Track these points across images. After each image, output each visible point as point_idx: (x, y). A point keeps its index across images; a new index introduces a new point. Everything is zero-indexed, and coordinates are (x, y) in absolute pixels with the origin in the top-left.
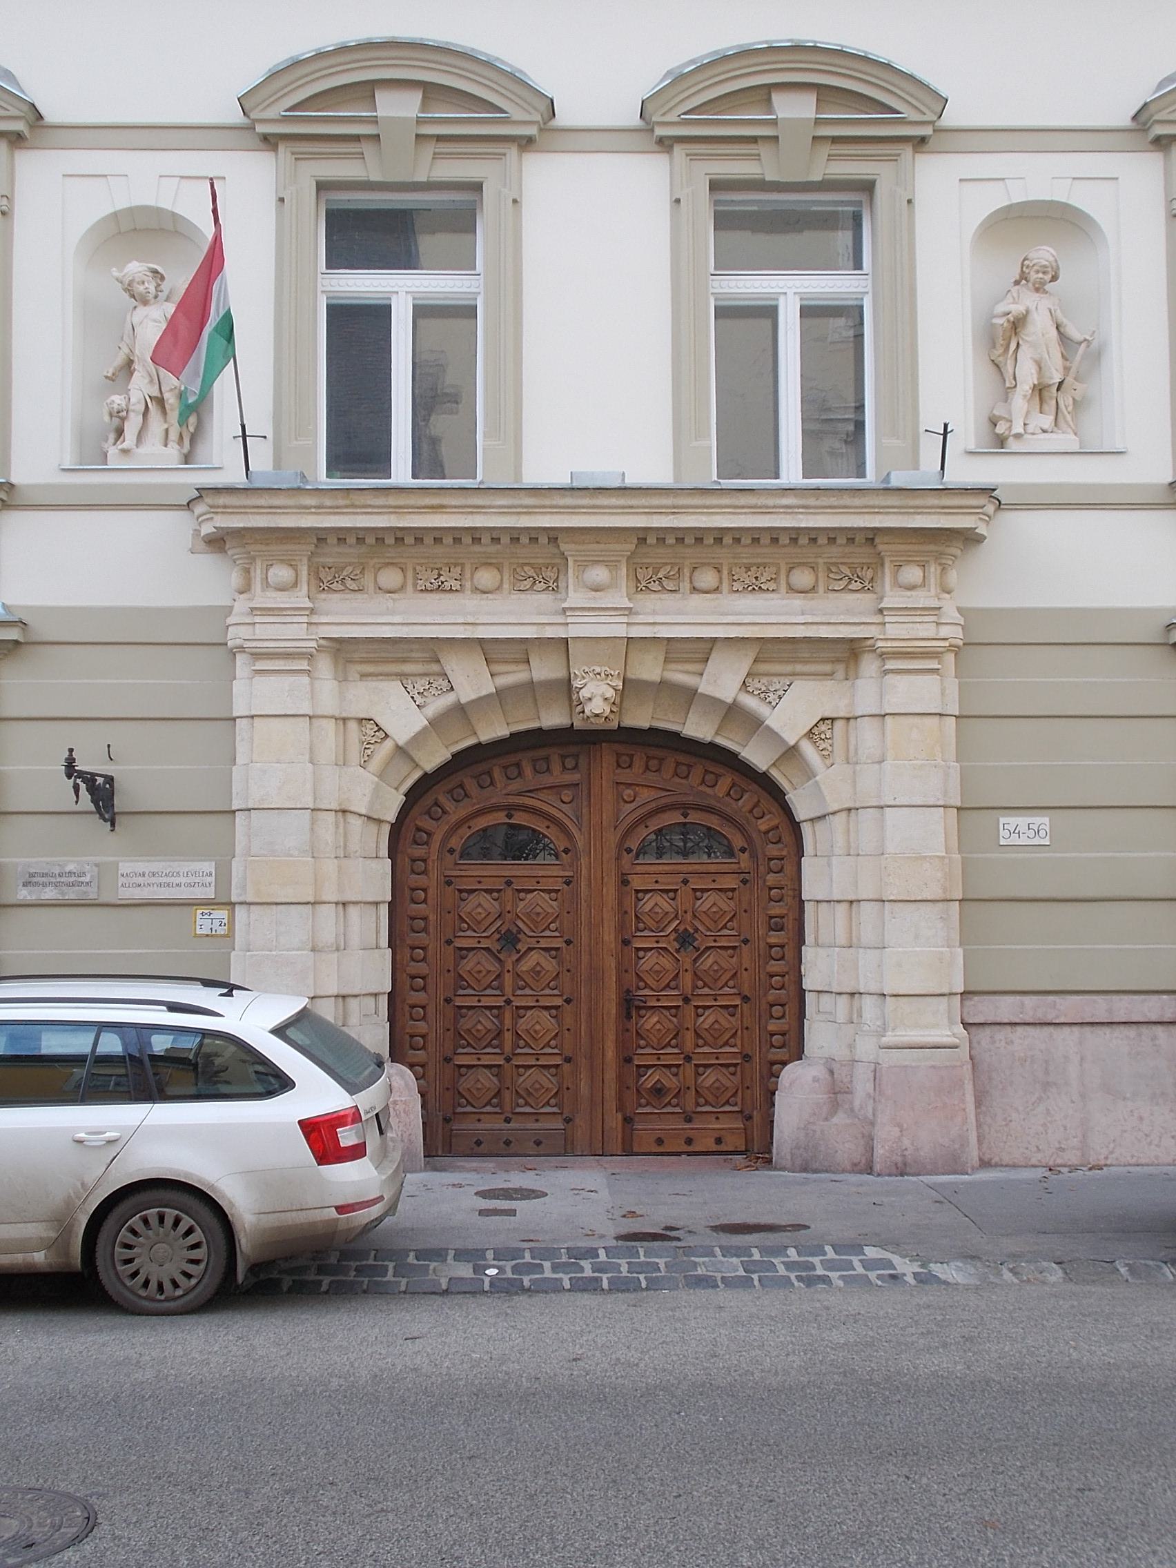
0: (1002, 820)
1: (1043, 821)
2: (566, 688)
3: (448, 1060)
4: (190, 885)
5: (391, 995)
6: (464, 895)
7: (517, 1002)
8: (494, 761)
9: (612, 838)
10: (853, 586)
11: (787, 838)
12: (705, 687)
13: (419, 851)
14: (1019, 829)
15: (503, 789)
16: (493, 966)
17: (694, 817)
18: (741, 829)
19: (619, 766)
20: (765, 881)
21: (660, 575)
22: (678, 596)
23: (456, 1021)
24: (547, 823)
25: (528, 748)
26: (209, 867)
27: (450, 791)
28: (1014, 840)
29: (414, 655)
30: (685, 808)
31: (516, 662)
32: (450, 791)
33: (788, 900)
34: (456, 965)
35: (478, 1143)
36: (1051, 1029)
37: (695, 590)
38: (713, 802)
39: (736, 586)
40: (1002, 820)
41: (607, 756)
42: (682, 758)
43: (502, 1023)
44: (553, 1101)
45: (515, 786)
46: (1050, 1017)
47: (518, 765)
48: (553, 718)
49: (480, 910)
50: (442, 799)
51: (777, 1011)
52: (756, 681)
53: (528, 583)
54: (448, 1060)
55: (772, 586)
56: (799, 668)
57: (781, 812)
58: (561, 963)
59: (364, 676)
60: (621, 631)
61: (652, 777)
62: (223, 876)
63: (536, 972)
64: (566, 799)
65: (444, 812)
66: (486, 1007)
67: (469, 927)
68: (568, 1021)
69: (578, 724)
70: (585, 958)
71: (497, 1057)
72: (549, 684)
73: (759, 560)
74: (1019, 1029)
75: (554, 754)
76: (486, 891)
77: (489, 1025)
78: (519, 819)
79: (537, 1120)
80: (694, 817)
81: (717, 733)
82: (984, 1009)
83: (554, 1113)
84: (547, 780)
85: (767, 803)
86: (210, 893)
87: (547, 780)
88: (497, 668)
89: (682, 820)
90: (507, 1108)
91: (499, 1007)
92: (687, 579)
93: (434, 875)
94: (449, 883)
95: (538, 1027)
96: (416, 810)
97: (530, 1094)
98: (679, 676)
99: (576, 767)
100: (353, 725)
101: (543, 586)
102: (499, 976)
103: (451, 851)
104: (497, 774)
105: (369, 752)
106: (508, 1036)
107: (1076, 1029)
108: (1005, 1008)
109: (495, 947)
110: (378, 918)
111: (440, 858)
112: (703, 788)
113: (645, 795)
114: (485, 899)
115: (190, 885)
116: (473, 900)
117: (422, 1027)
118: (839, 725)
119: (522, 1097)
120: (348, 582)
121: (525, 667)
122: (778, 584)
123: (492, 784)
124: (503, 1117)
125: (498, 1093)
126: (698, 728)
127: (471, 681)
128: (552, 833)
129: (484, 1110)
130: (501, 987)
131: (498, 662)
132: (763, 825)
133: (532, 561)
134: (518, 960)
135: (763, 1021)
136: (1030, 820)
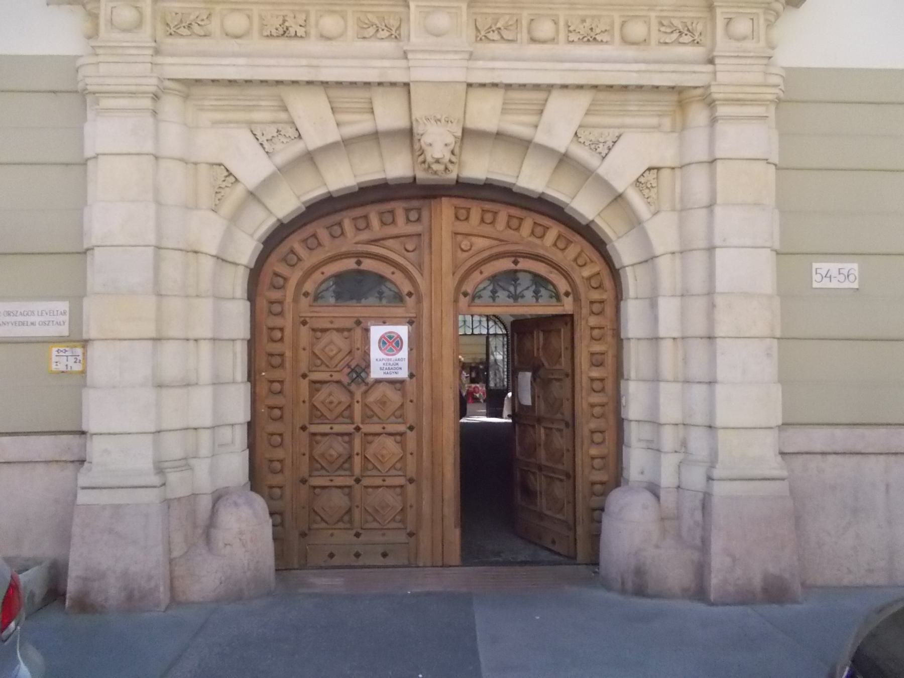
0: (815, 265)
1: (853, 267)
2: (409, 134)
3: (304, 481)
4: (44, 323)
5: (250, 424)
6: (319, 334)
7: (365, 429)
8: (344, 213)
9: (449, 283)
10: (686, 39)
11: (608, 283)
12: (541, 138)
13: (275, 295)
14: (833, 275)
15: (352, 238)
16: (344, 398)
17: (524, 264)
18: (566, 275)
19: (457, 218)
20: (587, 321)
21: (499, 25)
22: (515, 46)
23: (311, 447)
24: (393, 269)
25: (373, 202)
26: (64, 306)
27: (305, 241)
28: (826, 284)
29: (263, 103)
30: (516, 256)
31: (359, 111)
32: (305, 241)
33: (609, 339)
34: (312, 396)
35: (331, 555)
36: (859, 457)
37: (533, 40)
38: (541, 252)
39: (573, 37)
40: (815, 265)
41: (446, 208)
42: (514, 211)
43: (352, 447)
44: (398, 518)
45: (365, 236)
46: (860, 447)
47: (366, 217)
48: (397, 167)
49: (332, 346)
50: (298, 247)
51: (597, 437)
52: (587, 133)
53: (372, 31)
54: (304, 481)
55: (605, 37)
56: (628, 120)
57: (602, 260)
58: (404, 395)
59: (215, 123)
60: (460, 76)
61: (487, 229)
62: (76, 317)
63: (383, 403)
64: (410, 248)
65: (299, 259)
66: (338, 434)
67: (323, 362)
68: (411, 445)
69: (421, 175)
70: (426, 390)
71: (348, 479)
72: (393, 134)
73: (594, 12)
74: (831, 458)
75: (399, 207)
76: (338, 330)
77: (341, 449)
78: (368, 265)
79: (384, 535)
80: (524, 264)
81: (548, 186)
82: (799, 440)
83: (399, 529)
84: (391, 230)
85: (590, 252)
86: (64, 331)
87: (391, 230)
88: (343, 117)
89: (513, 266)
90: (357, 523)
91: (349, 434)
92: (525, 30)
93: (289, 316)
94: (304, 323)
95: (384, 452)
96: (273, 258)
97: (377, 511)
98: (516, 125)
99: (419, 220)
100: (203, 169)
101: (386, 34)
102: (349, 406)
103: (306, 294)
104: (347, 224)
105: (219, 196)
106: (357, 460)
107: (882, 458)
108: (818, 439)
109: (346, 380)
110: (235, 354)
111: (296, 300)
112: (532, 239)
113: (481, 243)
114: (336, 337)
115: (44, 323)
116: (326, 338)
117: (279, 454)
118: (665, 173)
119: (370, 514)
120: (195, 27)
121: (367, 117)
122: (612, 36)
123: (343, 234)
124: (354, 532)
125: (349, 511)
126: (532, 178)
127: (316, 122)
128: (398, 278)
129: (336, 526)
130: (351, 417)
131: (346, 111)
132: (586, 273)
133: (375, 9)
134: (366, 392)
135: (585, 446)
136: (840, 265)
